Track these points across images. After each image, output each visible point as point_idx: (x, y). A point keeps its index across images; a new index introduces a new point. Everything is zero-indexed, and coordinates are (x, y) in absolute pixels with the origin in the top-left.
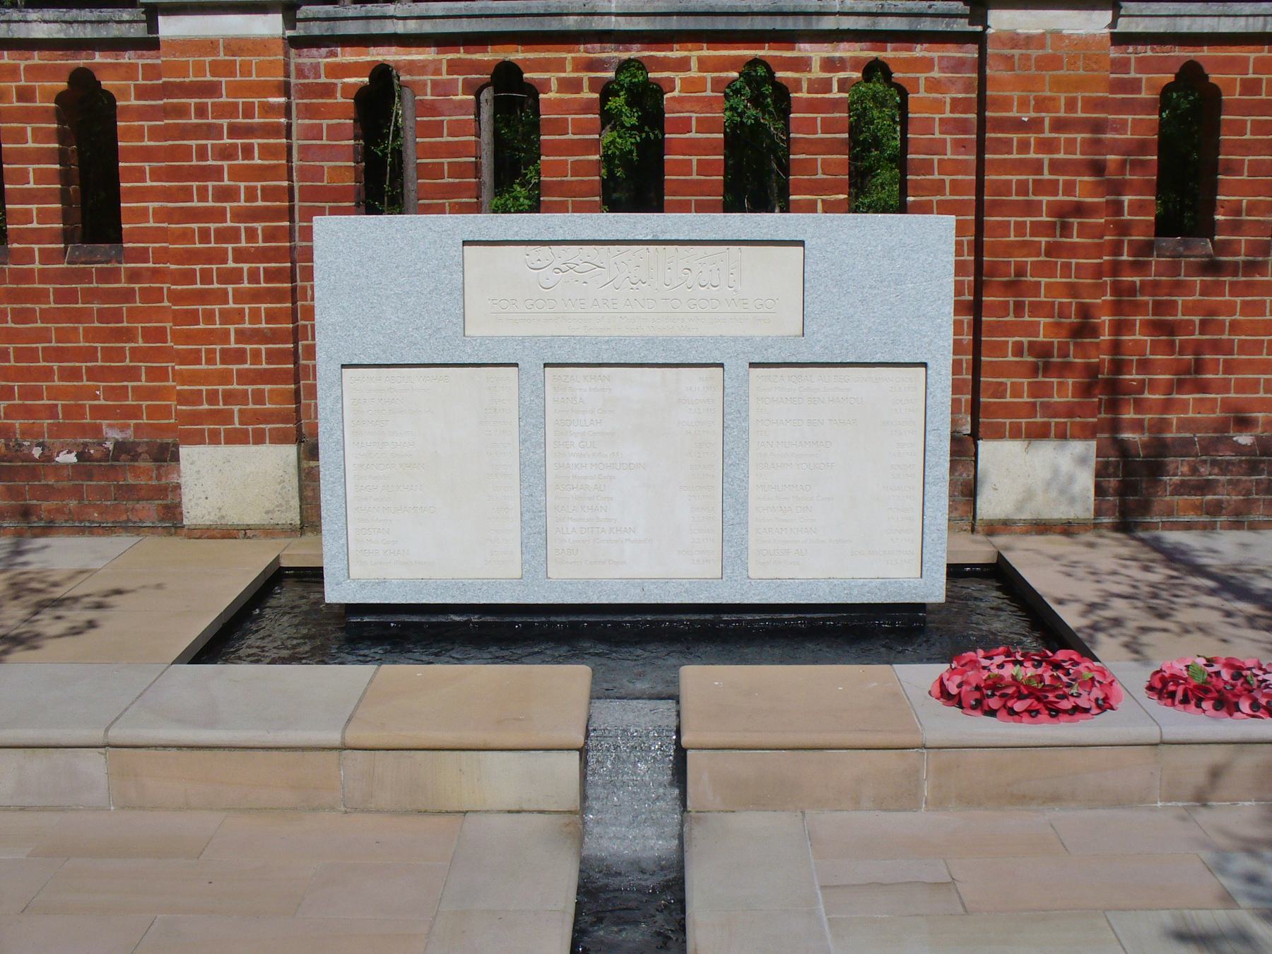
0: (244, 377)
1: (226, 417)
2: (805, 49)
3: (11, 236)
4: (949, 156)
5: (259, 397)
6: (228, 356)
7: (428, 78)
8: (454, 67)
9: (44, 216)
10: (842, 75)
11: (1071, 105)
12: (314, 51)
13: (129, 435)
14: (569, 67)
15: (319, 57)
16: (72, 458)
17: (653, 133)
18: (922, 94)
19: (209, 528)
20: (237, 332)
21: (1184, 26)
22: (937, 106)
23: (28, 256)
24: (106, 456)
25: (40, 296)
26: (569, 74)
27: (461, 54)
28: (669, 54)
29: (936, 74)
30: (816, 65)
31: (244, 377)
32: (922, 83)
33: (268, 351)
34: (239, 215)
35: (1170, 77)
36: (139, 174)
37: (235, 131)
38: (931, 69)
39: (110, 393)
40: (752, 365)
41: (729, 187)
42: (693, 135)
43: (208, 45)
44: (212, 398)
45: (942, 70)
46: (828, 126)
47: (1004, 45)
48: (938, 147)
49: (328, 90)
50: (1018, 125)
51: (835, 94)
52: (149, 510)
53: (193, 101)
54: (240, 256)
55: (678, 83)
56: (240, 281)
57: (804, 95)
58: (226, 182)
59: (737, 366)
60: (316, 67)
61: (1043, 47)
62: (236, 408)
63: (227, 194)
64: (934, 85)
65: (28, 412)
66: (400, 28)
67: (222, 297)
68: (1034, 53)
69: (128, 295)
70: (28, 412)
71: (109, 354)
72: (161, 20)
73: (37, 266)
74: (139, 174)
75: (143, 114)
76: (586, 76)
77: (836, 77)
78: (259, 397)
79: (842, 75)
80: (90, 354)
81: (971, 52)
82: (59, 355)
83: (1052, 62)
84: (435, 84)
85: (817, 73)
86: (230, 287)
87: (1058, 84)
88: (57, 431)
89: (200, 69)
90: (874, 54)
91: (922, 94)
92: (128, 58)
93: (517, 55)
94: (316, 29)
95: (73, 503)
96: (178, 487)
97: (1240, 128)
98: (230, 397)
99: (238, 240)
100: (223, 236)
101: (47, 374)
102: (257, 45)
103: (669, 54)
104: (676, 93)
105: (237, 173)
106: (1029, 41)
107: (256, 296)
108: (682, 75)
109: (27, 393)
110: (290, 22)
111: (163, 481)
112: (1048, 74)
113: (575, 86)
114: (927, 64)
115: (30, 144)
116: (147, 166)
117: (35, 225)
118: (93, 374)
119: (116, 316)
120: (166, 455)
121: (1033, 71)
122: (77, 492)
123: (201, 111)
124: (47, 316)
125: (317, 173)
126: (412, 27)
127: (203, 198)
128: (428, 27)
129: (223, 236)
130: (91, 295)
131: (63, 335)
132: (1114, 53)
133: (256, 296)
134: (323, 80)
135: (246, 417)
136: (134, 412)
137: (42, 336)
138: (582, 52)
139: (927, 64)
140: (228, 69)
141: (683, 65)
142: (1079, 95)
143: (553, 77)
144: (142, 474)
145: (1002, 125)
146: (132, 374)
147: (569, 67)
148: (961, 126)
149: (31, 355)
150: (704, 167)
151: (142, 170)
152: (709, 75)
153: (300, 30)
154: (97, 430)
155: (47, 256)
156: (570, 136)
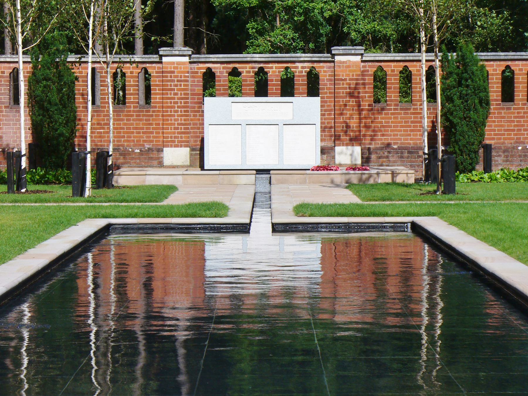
0: (178, 133)
1: (174, 142)
2: (297, 64)
3: (126, 103)
4: (328, 86)
5: (182, 137)
6: (175, 128)
7: (218, 70)
8: (224, 68)
9: (130, 98)
10: (305, 70)
11: (353, 75)
12: (194, 64)
13: (151, 146)
14: (248, 68)
15: (195, 66)
16: (139, 151)
17: (265, 77)
18: (322, 73)
19: (169, 166)
20: (177, 123)
21: (377, 59)
22: (326, 76)
23: (130, 107)
24: (146, 151)
25: (132, 116)
26: (248, 70)
27: (225, 65)
28: (269, 65)
29: (325, 69)
30: (300, 67)
31: (178, 133)
32: (322, 71)
33: (184, 128)
34: (178, 99)
35: (376, 69)
36: (155, 90)
37: (178, 81)
38: (324, 68)
39: (147, 137)
40: (284, 125)
41: (282, 89)
42: (274, 82)
43: (173, 63)
44: (171, 137)
45: (326, 68)
46: (303, 80)
47: (338, 63)
48: (326, 85)
49: (197, 73)
50: (342, 80)
51: (304, 74)
52: (155, 163)
53: (169, 75)
54: (178, 107)
55: (271, 71)
56: (178, 112)
57: (297, 74)
58: (176, 92)
59: (281, 125)
60: (194, 68)
61: (347, 63)
62: (176, 140)
63: (176, 94)
64: (325, 72)
65: (128, 141)
66: (213, 60)
67: (174, 116)
68: (345, 65)
69: (152, 116)
70: (128, 141)
71: (147, 128)
72: (163, 58)
73: (132, 109)
74: (155, 90)
75: (157, 77)
76: (252, 70)
77: (304, 70)
78: (182, 137)
79: (305, 70)
80: (143, 128)
81: (332, 64)
82: (136, 128)
83: (349, 67)
84: (220, 71)
85: (300, 69)
86: (176, 114)
87: (350, 71)
88: (135, 145)
89: (171, 68)
90: (312, 65)
91: (322, 73)
92: (154, 65)
93: (237, 65)
94: (195, 60)
95: (138, 161)
96: (162, 157)
97: (391, 79)
98: (175, 137)
99: (178, 104)
100: (175, 103)
101: (133, 133)
102: (183, 63)
103: (269, 65)
104: (270, 74)
105: (178, 90)
106: (344, 62)
107: (181, 116)
108: (272, 70)
109: (128, 137)
110: (190, 59)
111: (159, 156)
112: (348, 69)
113: (249, 72)
114: (323, 67)
115: (132, 83)
116: (157, 88)
117: (132, 100)
118: (143, 133)
119: (149, 120)
120: (160, 150)
121: (345, 69)
122: (139, 159)
123: (171, 77)
124: (134, 120)
125: (194, 90)
126: (215, 60)
127: (171, 95)
128: (219, 60)
129: (175, 103)
130: (144, 116)
131: (137, 124)
132: (363, 64)
133: (181, 116)
134: (196, 70)
135: (179, 142)
136: (152, 141)
137: (132, 124)
138: (251, 65)
139: (323, 67)
140: (177, 68)
141: (272, 68)
142: (355, 73)
143: (244, 70)
144: (154, 155)
145: (339, 80)
146: (152, 133)
147: (248, 68)
148: (331, 80)
149: (130, 128)
150: (276, 89)
151: (156, 89)
152: (277, 70)
153: (192, 60)
154: (143, 145)
155: (134, 107)
156: (248, 83)
